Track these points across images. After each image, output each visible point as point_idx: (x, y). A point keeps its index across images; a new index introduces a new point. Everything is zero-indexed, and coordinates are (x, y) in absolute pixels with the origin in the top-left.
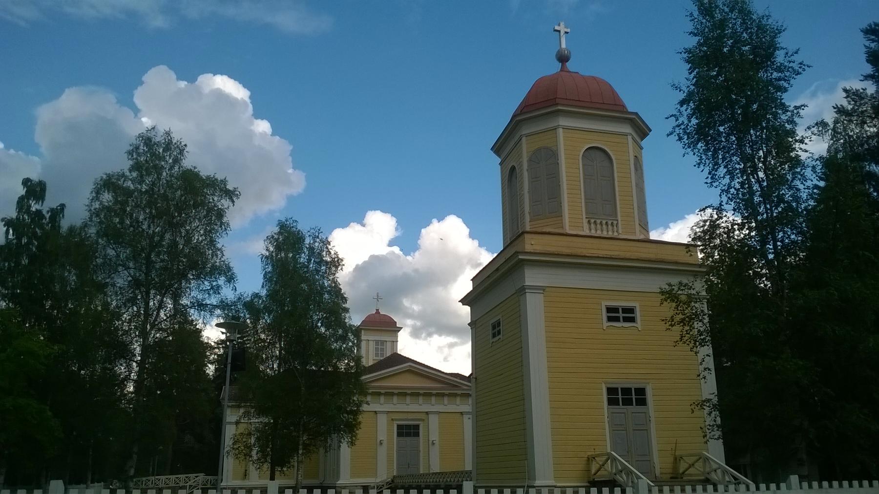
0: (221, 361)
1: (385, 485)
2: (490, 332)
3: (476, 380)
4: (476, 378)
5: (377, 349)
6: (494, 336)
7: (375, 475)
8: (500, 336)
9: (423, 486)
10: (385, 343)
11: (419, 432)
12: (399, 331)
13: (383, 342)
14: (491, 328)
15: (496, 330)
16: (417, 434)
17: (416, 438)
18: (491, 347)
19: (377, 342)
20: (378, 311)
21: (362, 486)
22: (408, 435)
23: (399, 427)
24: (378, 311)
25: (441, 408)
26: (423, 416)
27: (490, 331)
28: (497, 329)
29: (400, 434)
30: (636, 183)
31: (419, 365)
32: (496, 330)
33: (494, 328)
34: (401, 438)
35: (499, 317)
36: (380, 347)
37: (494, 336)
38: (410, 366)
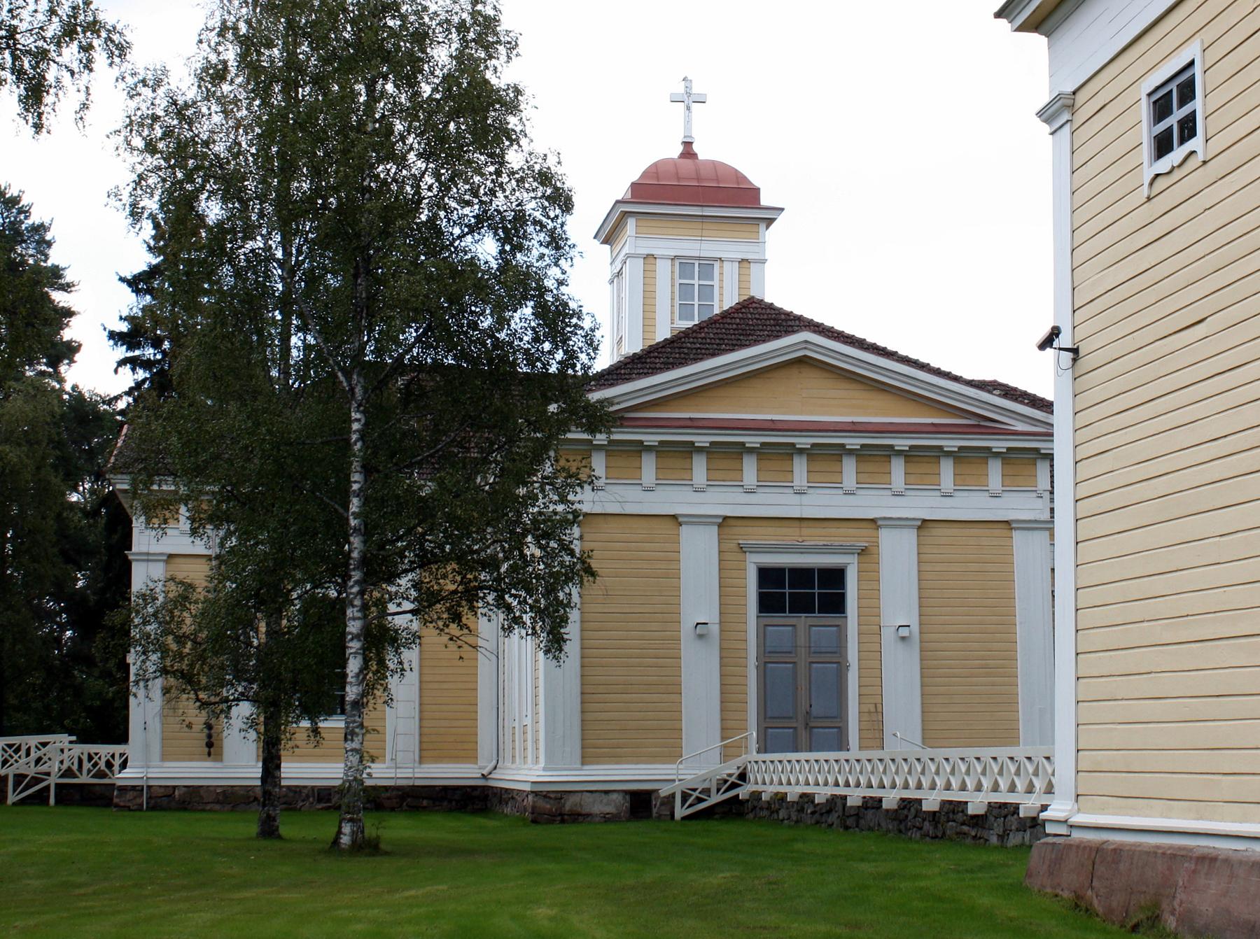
0: (47, 293)
1: (714, 790)
2: (1145, 132)
3: (1074, 360)
4: (1075, 351)
5: (686, 290)
6: (1163, 146)
7: (673, 753)
8: (1194, 144)
9: (212, 749)
10: (717, 265)
11: (819, 570)
12: (770, 221)
13: (707, 265)
14: (1144, 111)
15: (1173, 120)
16: (836, 604)
17: (830, 618)
18: (1149, 199)
19: (684, 264)
20: (688, 151)
21: (626, 792)
22: (802, 605)
23: (768, 576)
24: (688, 151)
25: (923, 505)
26: (859, 538)
27: (1145, 125)
28: (1178, 114)
29: (768, 604)
30: (1198, 819)
31: (845, 343)
32: (1173, 120)
33: (1161, 108)
34: (777, 618)
35: (1192, 51)
36: (696, 282)
37: (1163, 146)
38: (806, 342)
